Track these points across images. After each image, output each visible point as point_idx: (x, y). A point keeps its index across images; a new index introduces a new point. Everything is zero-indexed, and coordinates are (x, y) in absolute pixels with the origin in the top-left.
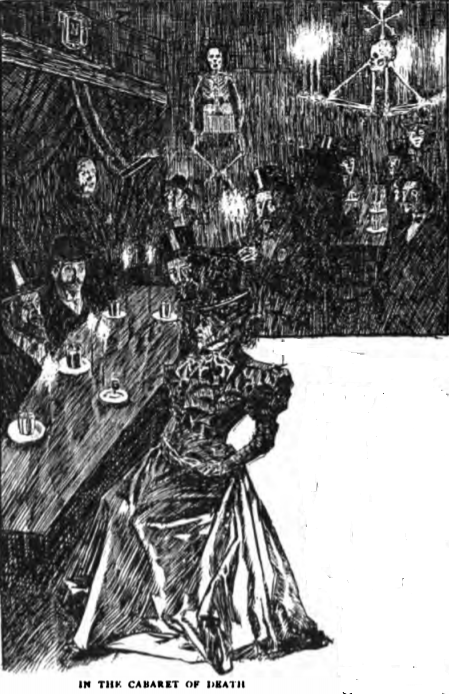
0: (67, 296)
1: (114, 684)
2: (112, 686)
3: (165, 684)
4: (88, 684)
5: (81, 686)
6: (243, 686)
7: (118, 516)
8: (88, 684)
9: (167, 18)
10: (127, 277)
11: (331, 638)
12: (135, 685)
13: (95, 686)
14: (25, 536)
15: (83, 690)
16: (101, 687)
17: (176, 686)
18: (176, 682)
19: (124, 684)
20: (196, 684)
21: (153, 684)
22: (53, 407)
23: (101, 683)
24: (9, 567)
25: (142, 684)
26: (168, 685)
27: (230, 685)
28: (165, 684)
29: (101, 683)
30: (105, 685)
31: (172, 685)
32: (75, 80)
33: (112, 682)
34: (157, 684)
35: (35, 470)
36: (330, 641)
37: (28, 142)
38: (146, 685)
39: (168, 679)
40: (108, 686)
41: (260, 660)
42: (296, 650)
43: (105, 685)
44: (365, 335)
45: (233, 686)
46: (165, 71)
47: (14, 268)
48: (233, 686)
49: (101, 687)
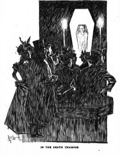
4: (43, 147)
6: (62, 148)
7: (108, 88)
8: (43, 147)
9: (87, 74)
10: (63, 95)
11: (108, 141)
13: (45, 147)
14: (6, 124)
16: (46, 148)
23: (46, 147)
25: (71, 147)
27: (59, 147)
29: (46, 147)
30: (47, 147)
37: (62, 52)
39: (76, 146)
43: (47, 147)
45: (60, 148)
48: (60, 148)
49: (46, 148)
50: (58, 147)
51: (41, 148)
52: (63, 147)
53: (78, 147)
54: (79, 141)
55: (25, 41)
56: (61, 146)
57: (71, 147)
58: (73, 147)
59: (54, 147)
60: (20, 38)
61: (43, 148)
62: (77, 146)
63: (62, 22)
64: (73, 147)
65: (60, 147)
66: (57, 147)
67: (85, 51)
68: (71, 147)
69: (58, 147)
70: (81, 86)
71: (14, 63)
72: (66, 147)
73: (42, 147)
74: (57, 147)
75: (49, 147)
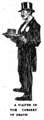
2: (13, 109)
3: (32, 110)
12: (24, 110)
16: (11, 111)
17: (36, 111)
18: (36, 109)
20: (13, 115)
23: (11, 109)
26: (34, 110)
27: (23, 115)
28: (32, 110)
29: (11, 109)
30: (12, 110)
31: (35, 110)
32: (30, 96)
34: (30, 110)
35: (29, 74)
36: (3, 34)
41: (17, 46)
42: (19, 74)
43: (25, 115)
46: (25, 60)
49: (11, 111)
50: (22, 115)
51: (34, 106)
52: (33, 105)
56: (35, 109)
59: (17, 114)
60: (26, 91)
65: (24, 114)
66: (21, 115)
67: (20, 90)
69: (22, 115)
71: (17, 97)
72: (23, 110)
73: (35, 104)
74: (21, 115)
75: (15, 110)
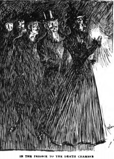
0: (77, 35)
1: (60, 156)
4: (22, 156)
5: (20, 157)
6: (75, 157)
8: (22, 156)
13: (24, 157)
15: (21, 158)
16: (26, 157)
19: (77, 157)
21: (70, 156)
22: (102, 27)
23: (26, 156)
24: (80, 55)
27: (71, 157)
29: (26, 156)
30: (27, 156)
33: (29, 156)
38: (89, 157)
40: (74, 157)
44: (100, 112)
45: (72, 157)
47: (46, 18)
48: (72, 157)
49: (57, 157)
52: (19, 156)
53: (93, 157)
54: (7, 149)
55: (95, 38)
57: (85, 156)
58: (88, 157)
61: (23, 157)
62: (91, 155)
63: (94, 70)
64: (29, 156)
65: (72, 156)
68: (85, 156)
70: (36, 100)
73: (21, 156)
